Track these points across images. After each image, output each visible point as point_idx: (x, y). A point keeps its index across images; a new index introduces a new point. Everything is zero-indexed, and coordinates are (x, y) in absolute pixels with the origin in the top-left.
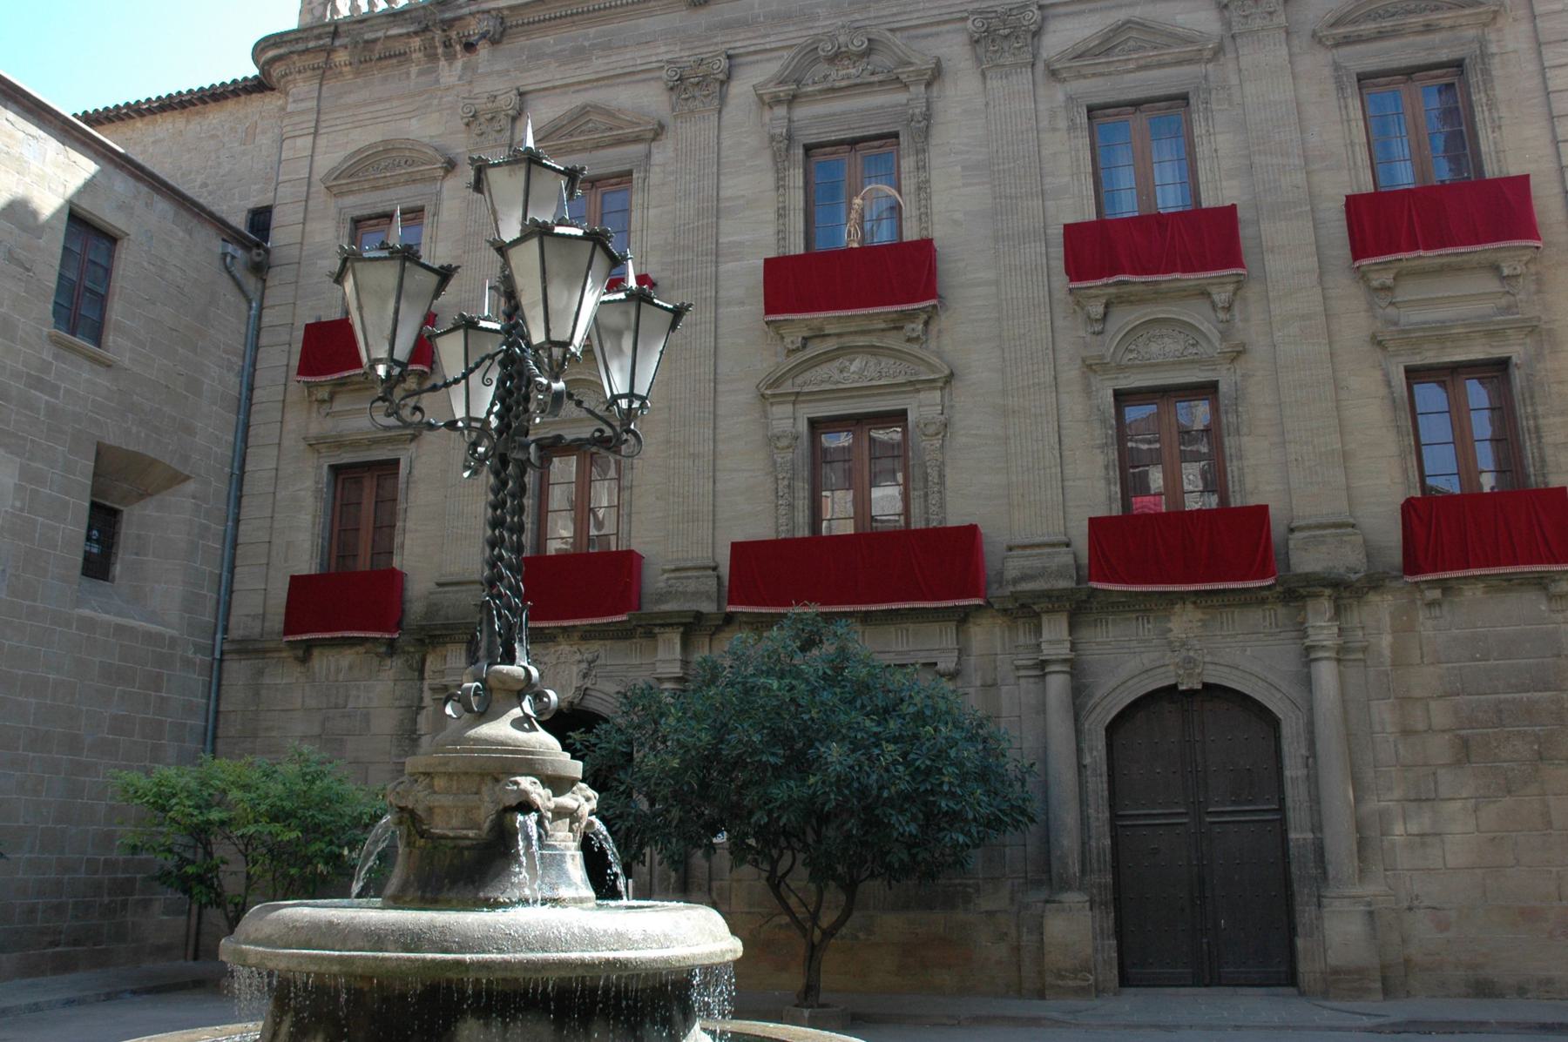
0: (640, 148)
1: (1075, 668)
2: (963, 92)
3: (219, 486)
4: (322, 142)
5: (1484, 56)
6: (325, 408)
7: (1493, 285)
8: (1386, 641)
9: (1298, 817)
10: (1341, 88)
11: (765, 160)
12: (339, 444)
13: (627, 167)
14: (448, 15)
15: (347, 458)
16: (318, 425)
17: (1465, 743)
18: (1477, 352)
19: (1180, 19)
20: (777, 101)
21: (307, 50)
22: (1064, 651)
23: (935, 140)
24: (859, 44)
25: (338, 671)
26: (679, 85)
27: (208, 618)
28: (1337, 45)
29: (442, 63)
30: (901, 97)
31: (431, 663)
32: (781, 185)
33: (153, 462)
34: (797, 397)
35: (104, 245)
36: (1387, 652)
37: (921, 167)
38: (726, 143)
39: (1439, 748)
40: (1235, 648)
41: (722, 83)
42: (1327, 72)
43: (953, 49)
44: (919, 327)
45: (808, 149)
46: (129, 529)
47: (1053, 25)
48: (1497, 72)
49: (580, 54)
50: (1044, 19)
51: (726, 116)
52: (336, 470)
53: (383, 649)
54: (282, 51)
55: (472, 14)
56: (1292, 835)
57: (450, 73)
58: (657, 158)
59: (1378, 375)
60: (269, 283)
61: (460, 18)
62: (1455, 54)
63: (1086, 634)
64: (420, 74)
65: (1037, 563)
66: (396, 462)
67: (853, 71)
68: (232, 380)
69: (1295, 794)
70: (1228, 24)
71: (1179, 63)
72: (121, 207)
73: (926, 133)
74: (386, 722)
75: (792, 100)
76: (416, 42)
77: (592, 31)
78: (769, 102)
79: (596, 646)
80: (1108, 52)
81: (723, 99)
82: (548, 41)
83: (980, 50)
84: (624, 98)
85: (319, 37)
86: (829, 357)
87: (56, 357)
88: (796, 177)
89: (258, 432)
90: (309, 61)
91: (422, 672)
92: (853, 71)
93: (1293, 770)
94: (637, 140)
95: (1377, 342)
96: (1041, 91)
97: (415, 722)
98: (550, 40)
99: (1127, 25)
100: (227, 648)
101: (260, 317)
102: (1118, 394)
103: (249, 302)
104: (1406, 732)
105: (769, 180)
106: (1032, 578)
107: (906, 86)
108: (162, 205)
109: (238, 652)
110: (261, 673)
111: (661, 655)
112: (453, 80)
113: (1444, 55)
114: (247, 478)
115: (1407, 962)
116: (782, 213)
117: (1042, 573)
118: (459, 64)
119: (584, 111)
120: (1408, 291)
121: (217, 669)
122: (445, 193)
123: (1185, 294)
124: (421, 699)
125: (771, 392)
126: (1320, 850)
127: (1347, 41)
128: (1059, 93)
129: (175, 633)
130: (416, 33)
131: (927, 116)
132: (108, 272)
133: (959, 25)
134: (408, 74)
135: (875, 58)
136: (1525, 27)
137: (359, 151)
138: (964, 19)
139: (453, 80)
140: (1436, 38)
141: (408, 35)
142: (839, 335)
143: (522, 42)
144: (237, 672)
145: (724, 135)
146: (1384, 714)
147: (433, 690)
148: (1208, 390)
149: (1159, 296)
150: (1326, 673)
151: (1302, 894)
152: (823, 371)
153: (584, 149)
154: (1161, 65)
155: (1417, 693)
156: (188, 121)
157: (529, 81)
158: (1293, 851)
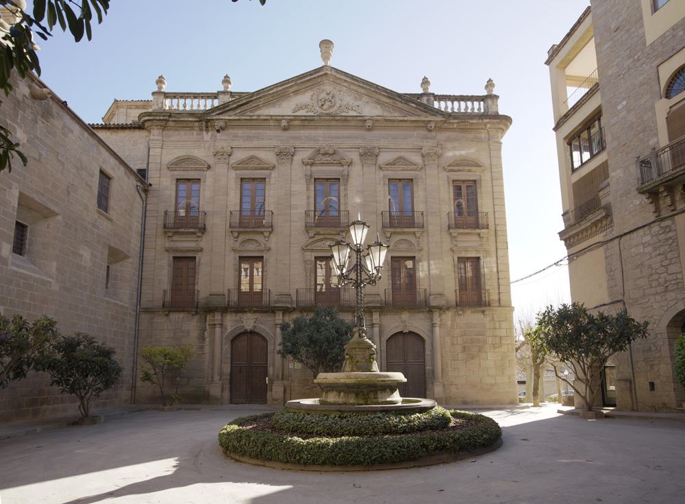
0: (268, 172)
1: (380, 326)
2: (356, 170)
3: (137, 260)
4: (164, 151)
5: (481, 180)
6: (170, 239)
7: (477, 239)
8: (450, 323)
9: (428, 363)
10: (449, 183)
11: (304, 181)
12: (176, 250)
13: (264, 177)
14: (209, 118)
15: (178, 255)
16: (168, 244)
17: (464, 347)
18: (473, 255)
19: (413, 158)
20: (307, 164)
21: (160, 120)
22: (378, 321)
23: (349, 182)
24: (331, 151)
25: (179, 318)
26: (280, 154)
27: (135, 301)
28: (449, 171)
29: (204, 132)
30: (341, 168)
31: (209, 317)
32: (308, 189)
33: (122, 252)
34: (312, 250)
35: (107, 180)
36: (449, 326)
37: (346, 189)
38: (293, 174)
39: (459, 348)
40: (417, 323)
41: (292, 156)
42: (446, 179)
43: (355, 156)
44: (344, 234)
45: (315, 179)
46: (110, 268)
47: (381, 154)
48: (483, 185)
49: (249, 138)
50: (379, 152)
51: (292, 165)
52: (174, 258)
53: (194, 313)
54: (151, 118)
55: (217, 119)
56: (427, 368)
57: (207, 136)
58: (273, 175)
59: (451, 258)
60: (149, 196)
61: (213, 120)
62: (475, 179)
63: (382, 317)
64: (197, 134)
65: (372, 299)
66: (195, 257)
67: (329, 159)
68: (139, 226)
69: (428, 358)
70: (424, 161)
71: (411, 170)
72: (112, 168)
73: (347, 180)
74: (195, 334)
75: (312, 164)
76: (197, 124)
77: (253, 132)
78: (304, 164)
79: (258, 314)
80: (394, 164)
81: (292, 160)
82: (240, 132)
83: (362, 158)
84: (262, 155)
85: (164, 116)
86: (321, 240)
87: (99, 217)
88: (312, 187)
89: (148, 244)
90: (159, 123)
91: (206, 320)
92: (329, 159)
93: (428, 352)
94: (267, 169)
95: (452, 250)
96: (377, 172)
97: (203, 334)
98: (240, 132)
99: (400, 158)
100: (143, 310)
101: (146, 207)
102: (316, 257)
103: (143, 201)
104: (453, 344)
105: (305, 187)
106: (370, 303)
107: (342, 166)
108: (122, 169)
109: (144, 312)
110: (152, 318)
111: (277, 318)
112: (208, 139)
113: (472, 178)
114: (144, 258)
115: (450, 397)
116: (308, 198)
117: (372, 302)
118: (210, 133)
119: (252, 157)
120: (461, 238)
121: (137, 317)
122: (207, 175)
123: (409, 233)
124: (206, 328)
125: (304, 249)
126: (433, 371)
127: (452, 171)
128: (382, 173)
129: (127, 305)
130: (197, 121)
131: (348, 175)
132: (108, 189)
133: (357, 150)
134: (193, 134)
135: (334, 156)
136: (490, 174)
137: (178, 158)
138: (359, 148)
139: (208, 139)
140: (471, 173)
141: (195, 121)
142: (323, 234)
143: (231, 131)
144: (144, 317)
145: (292, 171)
146: (448, 339)
147: (210, 325)
148: (413, 258)
149: (404, 233)
150: (437, 330)
151: (428, 380)
152: (319, 244)
153: (251, 169)
154: (408, 170)
155: (455, 335)
156: (111, 134)
157: (234, 144)
158: (427, 371)
